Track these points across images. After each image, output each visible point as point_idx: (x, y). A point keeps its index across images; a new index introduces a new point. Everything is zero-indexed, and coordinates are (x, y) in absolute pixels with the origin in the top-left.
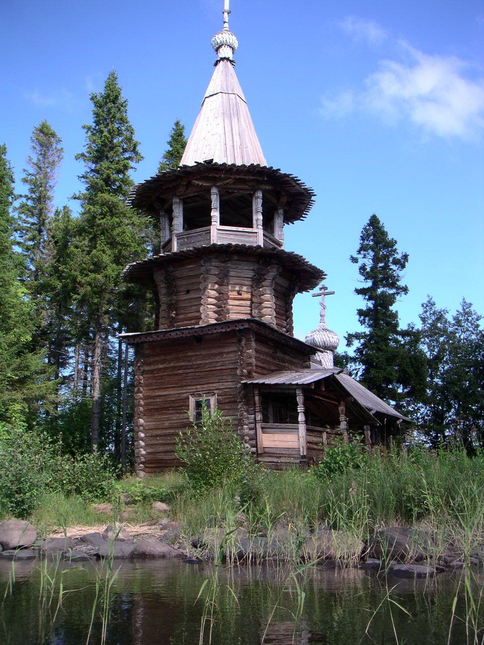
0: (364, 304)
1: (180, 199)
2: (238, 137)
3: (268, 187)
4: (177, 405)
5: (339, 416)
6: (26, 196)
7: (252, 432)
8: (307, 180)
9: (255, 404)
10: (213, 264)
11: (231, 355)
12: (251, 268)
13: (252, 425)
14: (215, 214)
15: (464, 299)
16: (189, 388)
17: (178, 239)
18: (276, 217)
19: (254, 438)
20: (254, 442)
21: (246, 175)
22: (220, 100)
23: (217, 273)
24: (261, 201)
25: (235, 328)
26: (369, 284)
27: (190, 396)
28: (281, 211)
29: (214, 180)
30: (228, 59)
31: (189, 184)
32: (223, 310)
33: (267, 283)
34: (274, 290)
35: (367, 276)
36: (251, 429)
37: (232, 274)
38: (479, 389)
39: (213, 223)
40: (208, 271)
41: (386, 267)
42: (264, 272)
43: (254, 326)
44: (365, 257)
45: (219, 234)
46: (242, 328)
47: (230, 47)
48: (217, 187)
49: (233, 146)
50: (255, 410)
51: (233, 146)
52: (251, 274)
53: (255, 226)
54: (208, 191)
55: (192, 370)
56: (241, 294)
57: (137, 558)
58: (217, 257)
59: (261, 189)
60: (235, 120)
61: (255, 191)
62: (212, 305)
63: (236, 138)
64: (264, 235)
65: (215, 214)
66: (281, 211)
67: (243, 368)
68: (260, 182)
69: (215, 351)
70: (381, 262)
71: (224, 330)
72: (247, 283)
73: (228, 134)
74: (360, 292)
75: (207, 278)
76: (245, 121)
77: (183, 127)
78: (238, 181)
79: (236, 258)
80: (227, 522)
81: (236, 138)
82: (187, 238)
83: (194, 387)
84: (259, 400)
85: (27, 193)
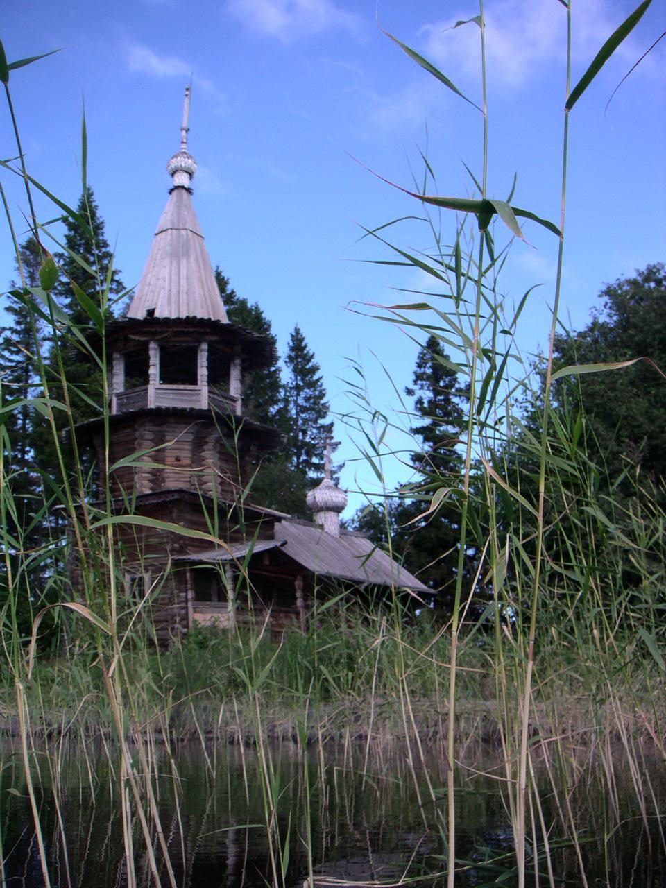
0: (419, 445)
1: (121, 355)
2: (185, 281)
3: (213, 338)
5: (295, 591)
6: (10, 329)
7: (183, 612)
9: (186, 581)
10: (147, 428)
13: (183, 605)
14: (154, 371)
18: (232, 369)
19: (185, 618)
20: (185, 622)
21: (185, 327)
22: (169, 237)
23: (152, 438)
24: (207, 354)
25: (165, 499)
26: (427, 421)
28: (238, 361)
29: (152, 335)
30: (183, 187)
31: (126, 339)
32: (157, 479)
33: (210, 446)
34: (219, 452)
35: (425, 412)
36: (182, 608)
39: (151, 382)
40: (142, 437)
41: (447, 401)
42: (204, 435)
43: (187, 496)
44: (422, 387)
45: (157, 394)
46: (172, 498)
47: (187, 172)
48: (156, 341)
49: (179, 292)
50: (186, 587)
51: (179, 292)
52: (191, 437)
53: (199, 382)
56: (179, 461)
59: (205, 341)
60: (184, 262)
61: (200, 342)
62: (148, 473)
63: (183, 282)
64: (209, 392)
65: (154, 371)
66: (238, 361)
67: (174, 542)
68: (205, 334)
70: (441, 395)
71: (155, 501)
72: (186, 447)
73: (174, 278)
74: (417, 431)
75: (142, 444)
76: (197, 261)
78: (177, 334)
79: (172, 420)
80: (477, 732)
81: (183, 282)
82: (127, 398)
84: (191, 577)
85: (13, 325)
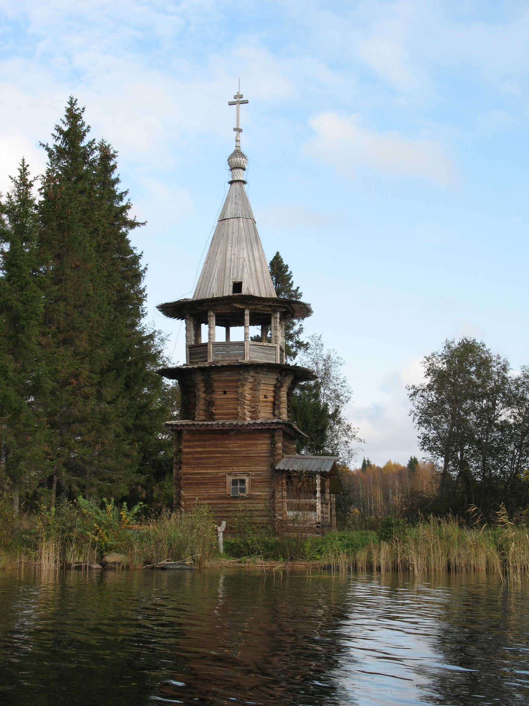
4: (215, 481)
8: (313, 307)
10: (251, 374)
11: (263, 446)
12: (275, 377)
15: (73, 116)
16: (226, 468)
17: (213, 347)
27: (227, 475)
37: (263, 382)
38: (146, 390)
40: (246, 379)
48: (250, 309)
54: (243, 310)
55: (229, 455)
57: (391, 552)
58: (253, 370)
61: (275, 311)
63: (258, 263)
69: (249, 442)
77: (107, 155)
83: (231, 468)
